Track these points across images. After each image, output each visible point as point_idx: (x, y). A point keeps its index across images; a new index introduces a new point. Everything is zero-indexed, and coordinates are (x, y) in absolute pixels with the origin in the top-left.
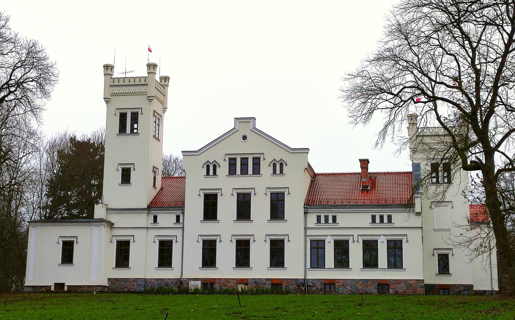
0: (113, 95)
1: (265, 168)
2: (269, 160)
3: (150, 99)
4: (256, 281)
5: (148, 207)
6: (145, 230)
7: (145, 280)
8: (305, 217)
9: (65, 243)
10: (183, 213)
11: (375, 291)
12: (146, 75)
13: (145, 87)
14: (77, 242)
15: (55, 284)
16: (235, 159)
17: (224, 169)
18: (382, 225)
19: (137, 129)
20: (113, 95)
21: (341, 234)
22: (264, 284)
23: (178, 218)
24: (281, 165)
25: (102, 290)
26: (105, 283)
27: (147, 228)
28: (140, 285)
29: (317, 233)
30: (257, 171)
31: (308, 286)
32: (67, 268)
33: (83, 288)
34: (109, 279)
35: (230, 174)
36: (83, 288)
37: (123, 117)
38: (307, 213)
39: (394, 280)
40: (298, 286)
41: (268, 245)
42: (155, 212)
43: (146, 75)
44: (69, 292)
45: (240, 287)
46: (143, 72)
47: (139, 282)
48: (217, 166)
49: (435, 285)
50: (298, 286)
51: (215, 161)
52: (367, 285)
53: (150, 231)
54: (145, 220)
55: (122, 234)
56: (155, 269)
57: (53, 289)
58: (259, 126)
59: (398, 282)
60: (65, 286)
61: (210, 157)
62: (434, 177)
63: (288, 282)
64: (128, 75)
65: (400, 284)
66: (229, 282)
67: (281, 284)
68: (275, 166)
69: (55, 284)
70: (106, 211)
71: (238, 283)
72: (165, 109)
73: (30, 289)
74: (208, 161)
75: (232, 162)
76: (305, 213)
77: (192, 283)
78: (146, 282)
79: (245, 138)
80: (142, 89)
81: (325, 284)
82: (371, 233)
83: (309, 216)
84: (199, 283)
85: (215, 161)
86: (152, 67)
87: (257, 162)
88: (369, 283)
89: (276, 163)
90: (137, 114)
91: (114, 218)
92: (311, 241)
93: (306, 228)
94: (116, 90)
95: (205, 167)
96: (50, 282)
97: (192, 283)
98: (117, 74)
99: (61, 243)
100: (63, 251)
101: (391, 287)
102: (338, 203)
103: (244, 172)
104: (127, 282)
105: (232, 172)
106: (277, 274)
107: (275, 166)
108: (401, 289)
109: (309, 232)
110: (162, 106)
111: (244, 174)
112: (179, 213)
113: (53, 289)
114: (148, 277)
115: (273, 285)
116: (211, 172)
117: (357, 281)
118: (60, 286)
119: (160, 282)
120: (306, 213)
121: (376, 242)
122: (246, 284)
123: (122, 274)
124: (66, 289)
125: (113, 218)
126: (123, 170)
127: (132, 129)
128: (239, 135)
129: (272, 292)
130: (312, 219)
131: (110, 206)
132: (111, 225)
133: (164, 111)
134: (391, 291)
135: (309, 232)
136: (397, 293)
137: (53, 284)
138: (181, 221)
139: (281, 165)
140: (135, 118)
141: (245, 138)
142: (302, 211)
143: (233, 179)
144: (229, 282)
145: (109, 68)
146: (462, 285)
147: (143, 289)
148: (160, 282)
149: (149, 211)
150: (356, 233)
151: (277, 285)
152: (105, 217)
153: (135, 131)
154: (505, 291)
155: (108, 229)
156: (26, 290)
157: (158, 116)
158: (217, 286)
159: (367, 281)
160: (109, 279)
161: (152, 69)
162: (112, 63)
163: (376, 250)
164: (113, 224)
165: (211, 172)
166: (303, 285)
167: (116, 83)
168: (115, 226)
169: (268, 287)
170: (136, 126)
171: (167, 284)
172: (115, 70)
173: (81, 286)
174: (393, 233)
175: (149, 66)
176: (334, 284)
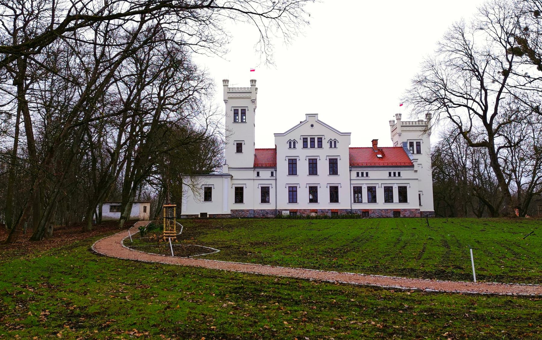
1: (325, 144)
4: (322, 211)
7: (254, 211)
8: (350, 173)
10: (276, 171)
11: (392, 216)
12: (402, 120)
13: (250, 94)
17: (300, 145)
18: (395, 178)
19: (245, 119)
21: (371, 183)
24: (335, 142)
26: (229, 212)
27: (254, 179)
28: (251, 214)
29: (357, 183)
30: (320, 146)
31: (353, 213)
32: (208, 203)
34: (231, 210)
37: (236, 112)
39: (403, 209)
40: (348, 213)
42: (258, 170)
45: (313, 214)
46: (249, 85)
50: (348, 213)
51: (294, 140)
52: (387, 213)
53: (255, 181)
54: (252, 174)
55: (239, 183)
57: (199, 216)
58: (320, 118)
59: (405, 210)
60: (353, 208)
61: (292, 137)
62: (55, 102)
65: (406, 211)
66: (306, 211)
67: (337, 213)
68: (331, 143)
73: (185, 217)
74: (331, 139)
75: (305, 141)
78: (254, 212)
79: (312, 126)
80: (248, 95)
81: (363, 212)
82: (389, 183)
83: (352, 172)
84: (288, 212)
85: (294, 140)
87: (320, 140)
88: (389, 211)
92: (354, 187)
93: (351, 180)
94: (231, 95)
96: (198, 213)
97: (283, 212)
99: (329, 187)
101: (401, 213)
102: (368, 165)
103: (313, 146)
105: (305, 146)
106: (334, 206)
107: (331, 143)
108: (407, 214)
109: (353, 182)
112: (273, 170)
114: (255, 209)
115: (332, 213)
117: (381, 210)
120: (350, 171)
121: (392, 187)
122: (316, 212)
124: (208, 216)
125: (232, 173)
127: (242, 119)
129: (332, 218)
130: (354, 174)
134: (401, 216)
135: (353, 182)
136: (405, 217)
138: (274, 175)
139: (335, 142)
140: (244, 112)
141: (312, 126)
142: (349, 169)
143: (305, 150)
144: (306, 211)
146: (428, 212)
147: (253, 216)
150: (380, 182)
151: (335, 212)
153: (244, 121)
156: (182, 217)
158: (298, 214)
159: (387, 210)
160: (231, 210)
161: (254, 83)
163: (392, 191)
166: (351, 212)
168: (233, 178)
169: (329, 214)
170: (244, 117)
171: (267, 213)
172: (229, 82)
174: (402, 183)
175: (252, 81)
176: (368, 212)
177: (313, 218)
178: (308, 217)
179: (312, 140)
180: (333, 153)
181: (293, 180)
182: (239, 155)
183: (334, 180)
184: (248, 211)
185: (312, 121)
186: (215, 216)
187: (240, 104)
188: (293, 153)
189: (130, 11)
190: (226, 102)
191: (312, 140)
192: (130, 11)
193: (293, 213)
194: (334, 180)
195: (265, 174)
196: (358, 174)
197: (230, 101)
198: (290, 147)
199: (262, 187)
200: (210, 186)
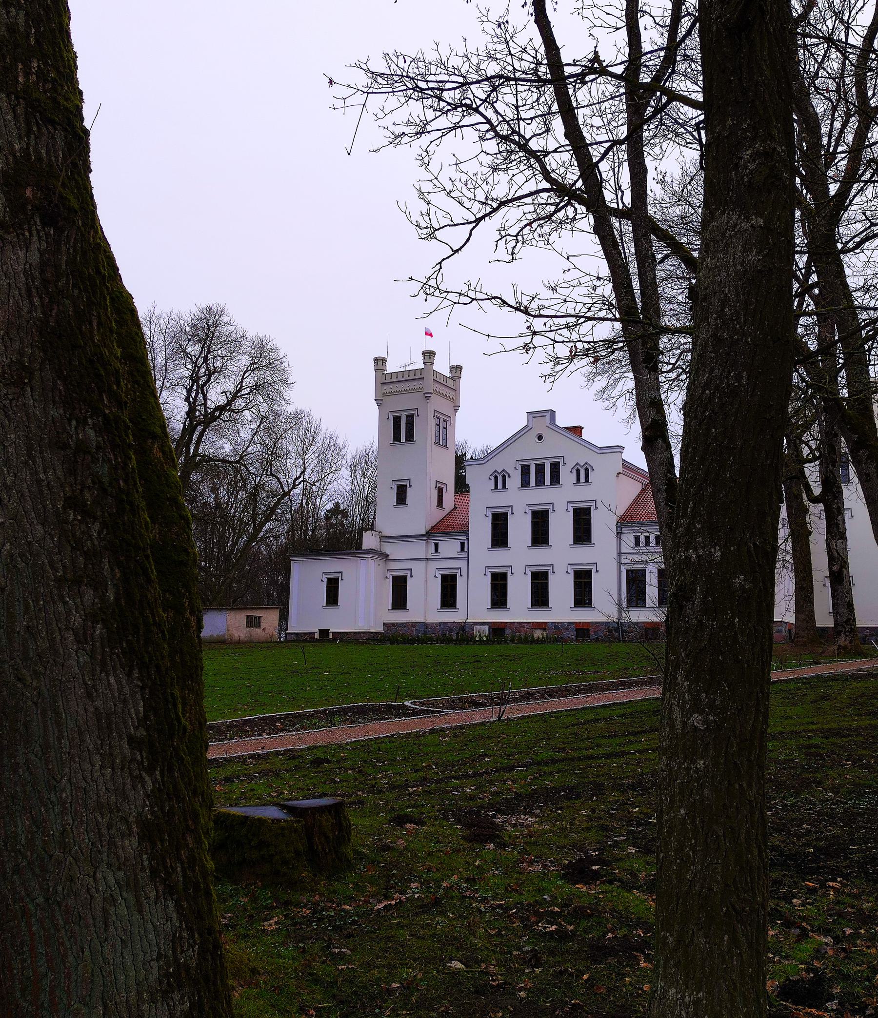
0: (385, 395)
1: (566, 476)
2: (571, 464)
3: (427, 397)
4: (556, 626)
5: (427, 533)
6: (424, 562)
9: (329, 581)
10: (468, 539)
12: (422, 366)
14: (342, 579)
15: (320, 630)
16: (543, 465)
17: (515, 480)
20: (385, 395)
22: (566, 629)
23: (462, 544)
24: (587, 470)
25: (370, 639)
26: (381, 629)
27: (427, 559)
30: (555, 479)
31: (623, 631)
32: (331, 610)
33: (349, 636)
35: (522, 486)
36: (349, 636)
37: (397, 421)
38: (621, 533)
40: (610, 631)
41: (488, 580)
42: (436, 539)
43: (422, 366)
44: (334, 640)
45: (538, 634)
47: (417, 628)
48: (590, 470)
49: (827, 628)
50: (610, 631)
51: (504, 470)
53: (431, 563)
54: (420, 549)
56: (436, 610)
57: (317, 636)
61: (498, 465)
63: (597, 627)
64: (408, 369)
66: (523, 627)
68: (578, 471)
69: (320, 630)
70: (378, 540)
71: (535, 629)
72: (456, 408)
73: (294, 637)
74: (496, 471)
76: (618, 533)
77: (477, 627)
79: (540, 437)
80: (416, 384)
83: (623, 537)
85: (504, 470)
86: (428, 356)
87: (555, 467)
89: (579, 468)
90: (412, 416)
91: (389, 548)
92: (628, 572)
93: (620, 554)
94: (388, 388)
95: (574, 472)
96: (314, 629)
98: (392, 367)
99: (325, 580)
100: (442, 586)
103: (540, 482)
104: (405, 627)
105: (525, 483)
106: (583, 616)
110: (452, 404)
111: (539, 486)
112: (462, 538)
113: (317, 636)
114: (429, 621)
116: (583, 479)
118: (324, 632)
119: (442, 626)
120: (619, 534)
122: (545, 629)
123: (399, 617)
124: (331, 636)
125: (388, 548)
126: (398, 487)
128: (533, 435)
130: (629, 539)
131: (385, 533)
132: (385, 557)
133: (456, 411)
137: (317, 631)
138: (466, 550)
139: (587, 470)
141: (540, 437)
144: (523, 627)
145: (380, 362)
146: (867, 628)
148: (442, 626)
149: (429, 537)
152: (378, 547)
154: (799, 639)
155: (382, 562)
157: (442, 417)
158: (508, 632)
162: (384, 355)
164: (388, 555)
165: (583, 479)
166: (617, 630)
167: (388, 380)
168: (390, 558)
169: (572, 634)
171: (451, 630)
173: (347, 633)
177: (539, 641)
178: (529, 640)
179: (540, 468)
180: (583, 494)
181: (499, 558)
182: (401, 509)
183: (583, 556)
184: (414, 625)
185: (541, 427)
186: (358, 637)
187: (402, 404)
188: (500, 500)
189: (704, 141)
190: (379, 404)
191: (540, 468)
192: (704, 141)
193: (498, 630)
194: (583, 556)
195: (449, 547)
196: (637, 539)
197: (387, 399)
198: (578, 480)
199: (393, 577)
200: (454, 572)
